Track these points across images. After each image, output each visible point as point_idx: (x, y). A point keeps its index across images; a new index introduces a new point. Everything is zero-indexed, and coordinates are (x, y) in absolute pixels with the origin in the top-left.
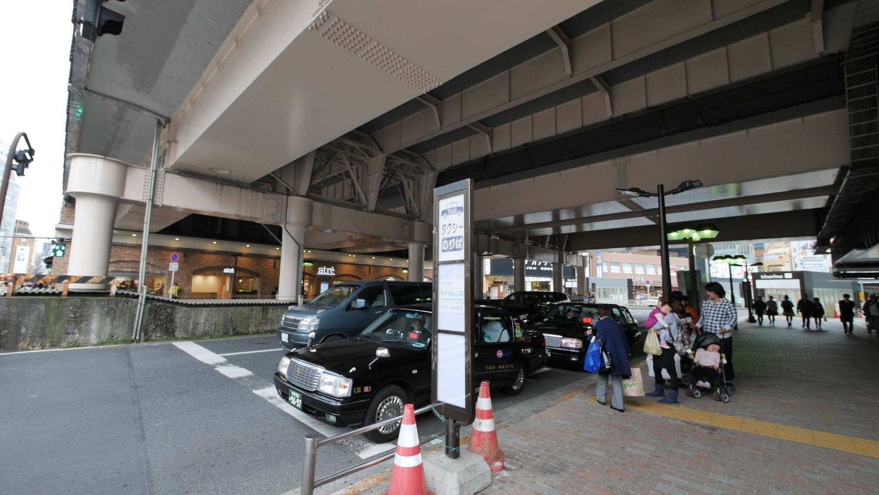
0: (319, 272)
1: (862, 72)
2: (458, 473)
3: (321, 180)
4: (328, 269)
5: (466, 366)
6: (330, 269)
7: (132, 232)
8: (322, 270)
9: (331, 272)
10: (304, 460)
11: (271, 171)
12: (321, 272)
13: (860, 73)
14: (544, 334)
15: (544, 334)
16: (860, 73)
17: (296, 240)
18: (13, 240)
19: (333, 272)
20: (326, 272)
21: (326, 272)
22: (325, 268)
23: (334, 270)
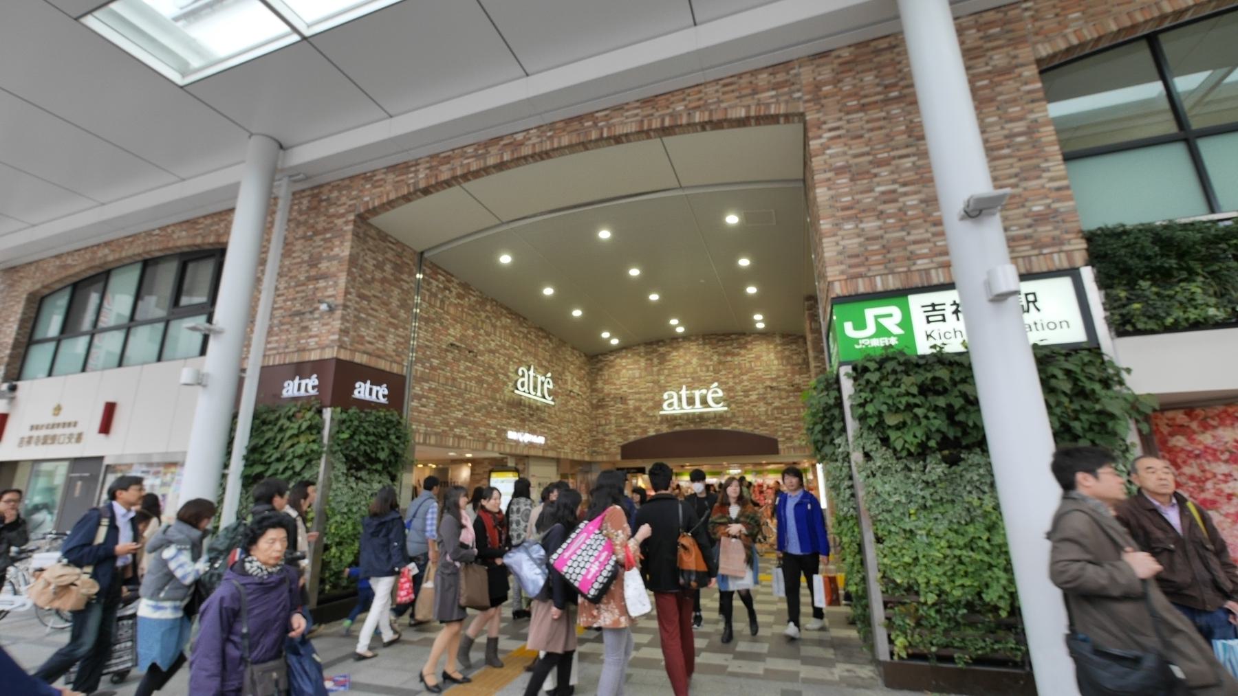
0: (356, 392)
9: (380, 396)
19: (384, 396)
22: (684, 393)
23: (720, 394)
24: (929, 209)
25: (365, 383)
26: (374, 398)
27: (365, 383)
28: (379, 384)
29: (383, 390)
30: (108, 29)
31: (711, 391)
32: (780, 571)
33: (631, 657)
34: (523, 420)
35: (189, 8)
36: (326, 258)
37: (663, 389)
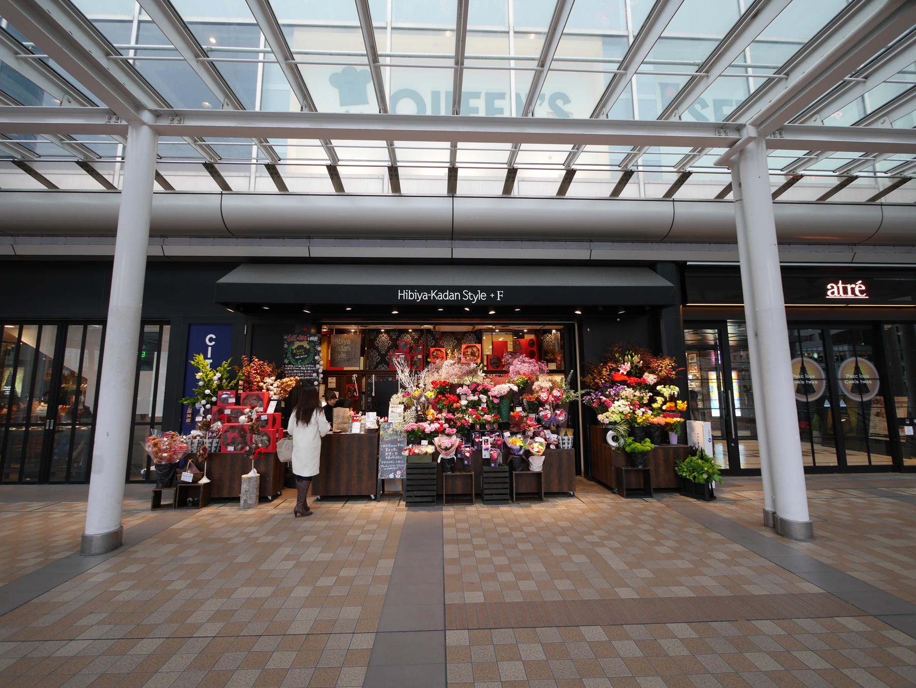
0: (829, 293)
1: (902, 279)
2: (407, 503)
3: (64, 427)
4: (849, 287)
5: (669, 440)
6: (853, 286)
7: (30, 368)
8: (835, 290)
9: (857, 292)
10: (874, 398)
11: (87, 516)
12: (833, 293)
13: (898, 279)
14: (845, 405)
15: (845, 405)
16: (898, 279)
17: (674, 222)
18: (376, 634)
19: (861, 292)
22: (840, 285)
23: (863, 288)
24: (594, 398)
25: (837, 283)
26: (850, 295)
27: (837, 283)
28: (854, 282)
29: (859, 286)
30: (634, 98)
31: (858, 286)
32: (391, 399)
33: (423, 397)
34: (662, 357)
35: (539, 89)
36: (273, 441)
37: (637, 422)
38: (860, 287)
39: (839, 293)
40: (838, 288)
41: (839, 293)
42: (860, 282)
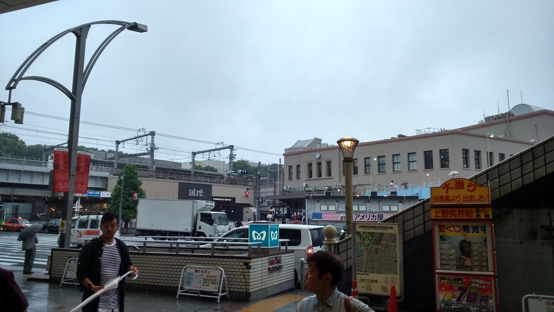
4: (198, 191)
6: (199, 191)
8: (192, 193)
12: (191, 194)
20: (196, 194)
21: (196, 194)
23: (202, 192)
25: (193, 190)
38: (201, 192)
39: (193, 194)
40: (193, 191)
41: (193, 194)
42: (202, 190)
